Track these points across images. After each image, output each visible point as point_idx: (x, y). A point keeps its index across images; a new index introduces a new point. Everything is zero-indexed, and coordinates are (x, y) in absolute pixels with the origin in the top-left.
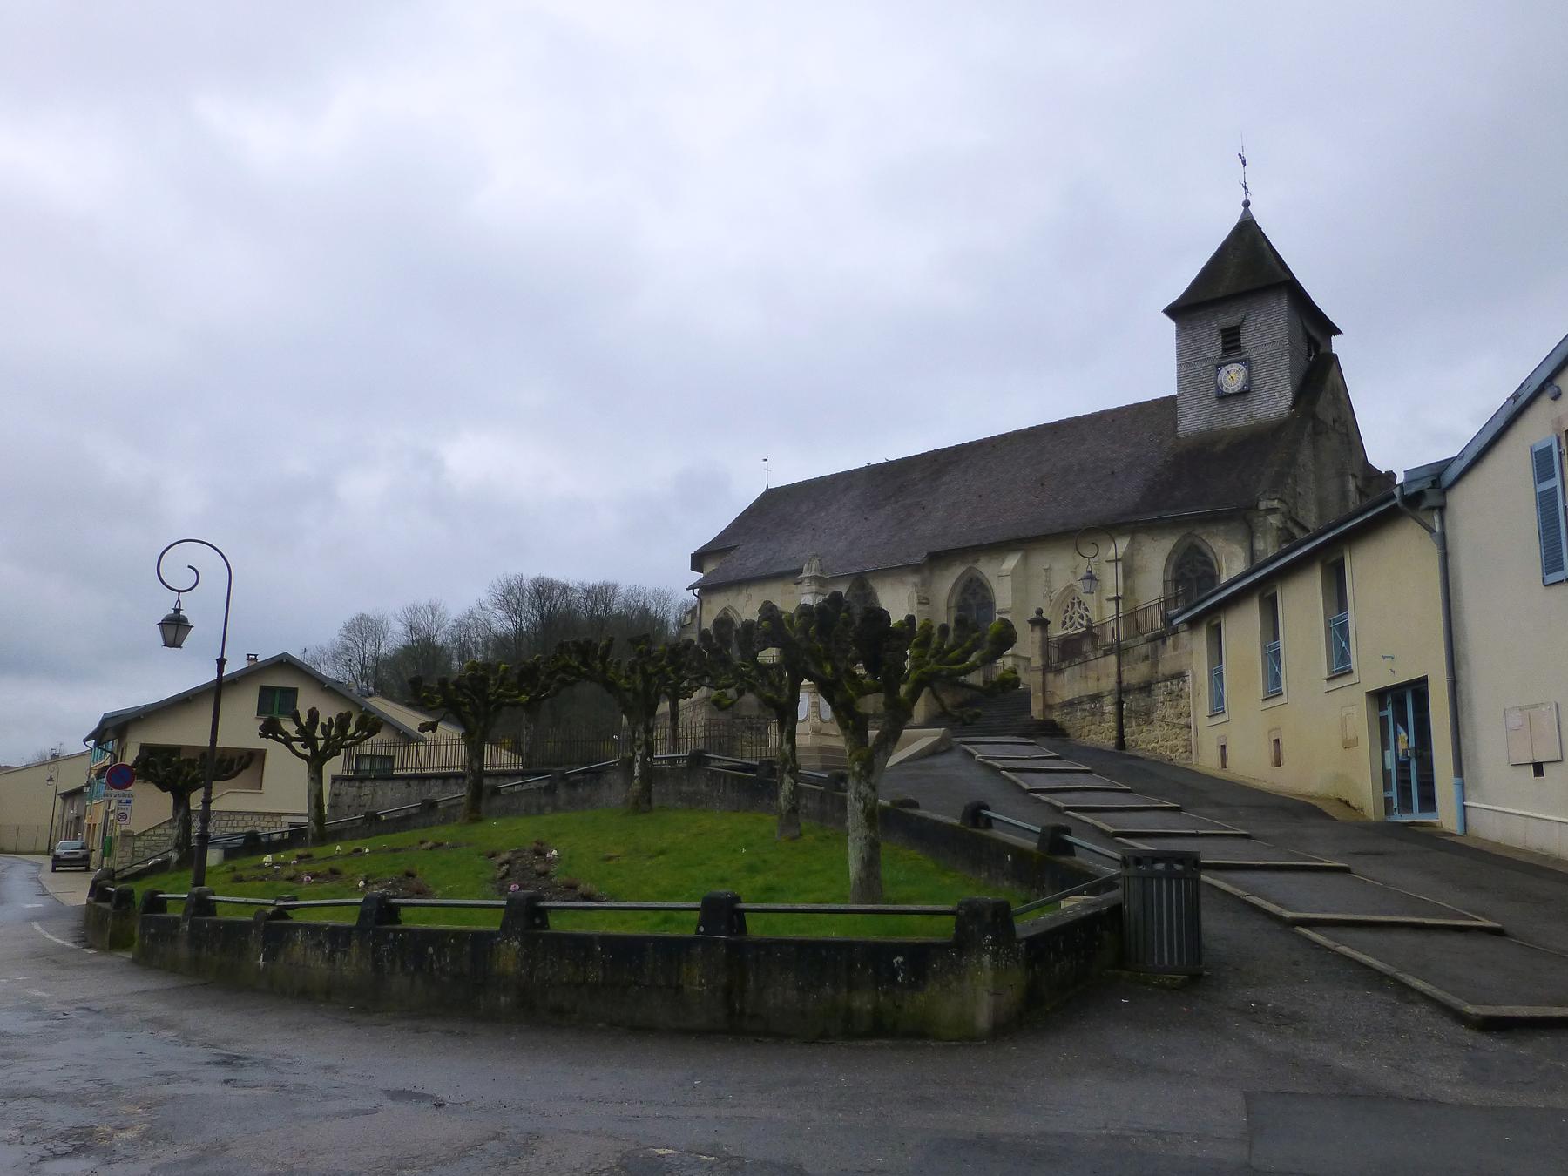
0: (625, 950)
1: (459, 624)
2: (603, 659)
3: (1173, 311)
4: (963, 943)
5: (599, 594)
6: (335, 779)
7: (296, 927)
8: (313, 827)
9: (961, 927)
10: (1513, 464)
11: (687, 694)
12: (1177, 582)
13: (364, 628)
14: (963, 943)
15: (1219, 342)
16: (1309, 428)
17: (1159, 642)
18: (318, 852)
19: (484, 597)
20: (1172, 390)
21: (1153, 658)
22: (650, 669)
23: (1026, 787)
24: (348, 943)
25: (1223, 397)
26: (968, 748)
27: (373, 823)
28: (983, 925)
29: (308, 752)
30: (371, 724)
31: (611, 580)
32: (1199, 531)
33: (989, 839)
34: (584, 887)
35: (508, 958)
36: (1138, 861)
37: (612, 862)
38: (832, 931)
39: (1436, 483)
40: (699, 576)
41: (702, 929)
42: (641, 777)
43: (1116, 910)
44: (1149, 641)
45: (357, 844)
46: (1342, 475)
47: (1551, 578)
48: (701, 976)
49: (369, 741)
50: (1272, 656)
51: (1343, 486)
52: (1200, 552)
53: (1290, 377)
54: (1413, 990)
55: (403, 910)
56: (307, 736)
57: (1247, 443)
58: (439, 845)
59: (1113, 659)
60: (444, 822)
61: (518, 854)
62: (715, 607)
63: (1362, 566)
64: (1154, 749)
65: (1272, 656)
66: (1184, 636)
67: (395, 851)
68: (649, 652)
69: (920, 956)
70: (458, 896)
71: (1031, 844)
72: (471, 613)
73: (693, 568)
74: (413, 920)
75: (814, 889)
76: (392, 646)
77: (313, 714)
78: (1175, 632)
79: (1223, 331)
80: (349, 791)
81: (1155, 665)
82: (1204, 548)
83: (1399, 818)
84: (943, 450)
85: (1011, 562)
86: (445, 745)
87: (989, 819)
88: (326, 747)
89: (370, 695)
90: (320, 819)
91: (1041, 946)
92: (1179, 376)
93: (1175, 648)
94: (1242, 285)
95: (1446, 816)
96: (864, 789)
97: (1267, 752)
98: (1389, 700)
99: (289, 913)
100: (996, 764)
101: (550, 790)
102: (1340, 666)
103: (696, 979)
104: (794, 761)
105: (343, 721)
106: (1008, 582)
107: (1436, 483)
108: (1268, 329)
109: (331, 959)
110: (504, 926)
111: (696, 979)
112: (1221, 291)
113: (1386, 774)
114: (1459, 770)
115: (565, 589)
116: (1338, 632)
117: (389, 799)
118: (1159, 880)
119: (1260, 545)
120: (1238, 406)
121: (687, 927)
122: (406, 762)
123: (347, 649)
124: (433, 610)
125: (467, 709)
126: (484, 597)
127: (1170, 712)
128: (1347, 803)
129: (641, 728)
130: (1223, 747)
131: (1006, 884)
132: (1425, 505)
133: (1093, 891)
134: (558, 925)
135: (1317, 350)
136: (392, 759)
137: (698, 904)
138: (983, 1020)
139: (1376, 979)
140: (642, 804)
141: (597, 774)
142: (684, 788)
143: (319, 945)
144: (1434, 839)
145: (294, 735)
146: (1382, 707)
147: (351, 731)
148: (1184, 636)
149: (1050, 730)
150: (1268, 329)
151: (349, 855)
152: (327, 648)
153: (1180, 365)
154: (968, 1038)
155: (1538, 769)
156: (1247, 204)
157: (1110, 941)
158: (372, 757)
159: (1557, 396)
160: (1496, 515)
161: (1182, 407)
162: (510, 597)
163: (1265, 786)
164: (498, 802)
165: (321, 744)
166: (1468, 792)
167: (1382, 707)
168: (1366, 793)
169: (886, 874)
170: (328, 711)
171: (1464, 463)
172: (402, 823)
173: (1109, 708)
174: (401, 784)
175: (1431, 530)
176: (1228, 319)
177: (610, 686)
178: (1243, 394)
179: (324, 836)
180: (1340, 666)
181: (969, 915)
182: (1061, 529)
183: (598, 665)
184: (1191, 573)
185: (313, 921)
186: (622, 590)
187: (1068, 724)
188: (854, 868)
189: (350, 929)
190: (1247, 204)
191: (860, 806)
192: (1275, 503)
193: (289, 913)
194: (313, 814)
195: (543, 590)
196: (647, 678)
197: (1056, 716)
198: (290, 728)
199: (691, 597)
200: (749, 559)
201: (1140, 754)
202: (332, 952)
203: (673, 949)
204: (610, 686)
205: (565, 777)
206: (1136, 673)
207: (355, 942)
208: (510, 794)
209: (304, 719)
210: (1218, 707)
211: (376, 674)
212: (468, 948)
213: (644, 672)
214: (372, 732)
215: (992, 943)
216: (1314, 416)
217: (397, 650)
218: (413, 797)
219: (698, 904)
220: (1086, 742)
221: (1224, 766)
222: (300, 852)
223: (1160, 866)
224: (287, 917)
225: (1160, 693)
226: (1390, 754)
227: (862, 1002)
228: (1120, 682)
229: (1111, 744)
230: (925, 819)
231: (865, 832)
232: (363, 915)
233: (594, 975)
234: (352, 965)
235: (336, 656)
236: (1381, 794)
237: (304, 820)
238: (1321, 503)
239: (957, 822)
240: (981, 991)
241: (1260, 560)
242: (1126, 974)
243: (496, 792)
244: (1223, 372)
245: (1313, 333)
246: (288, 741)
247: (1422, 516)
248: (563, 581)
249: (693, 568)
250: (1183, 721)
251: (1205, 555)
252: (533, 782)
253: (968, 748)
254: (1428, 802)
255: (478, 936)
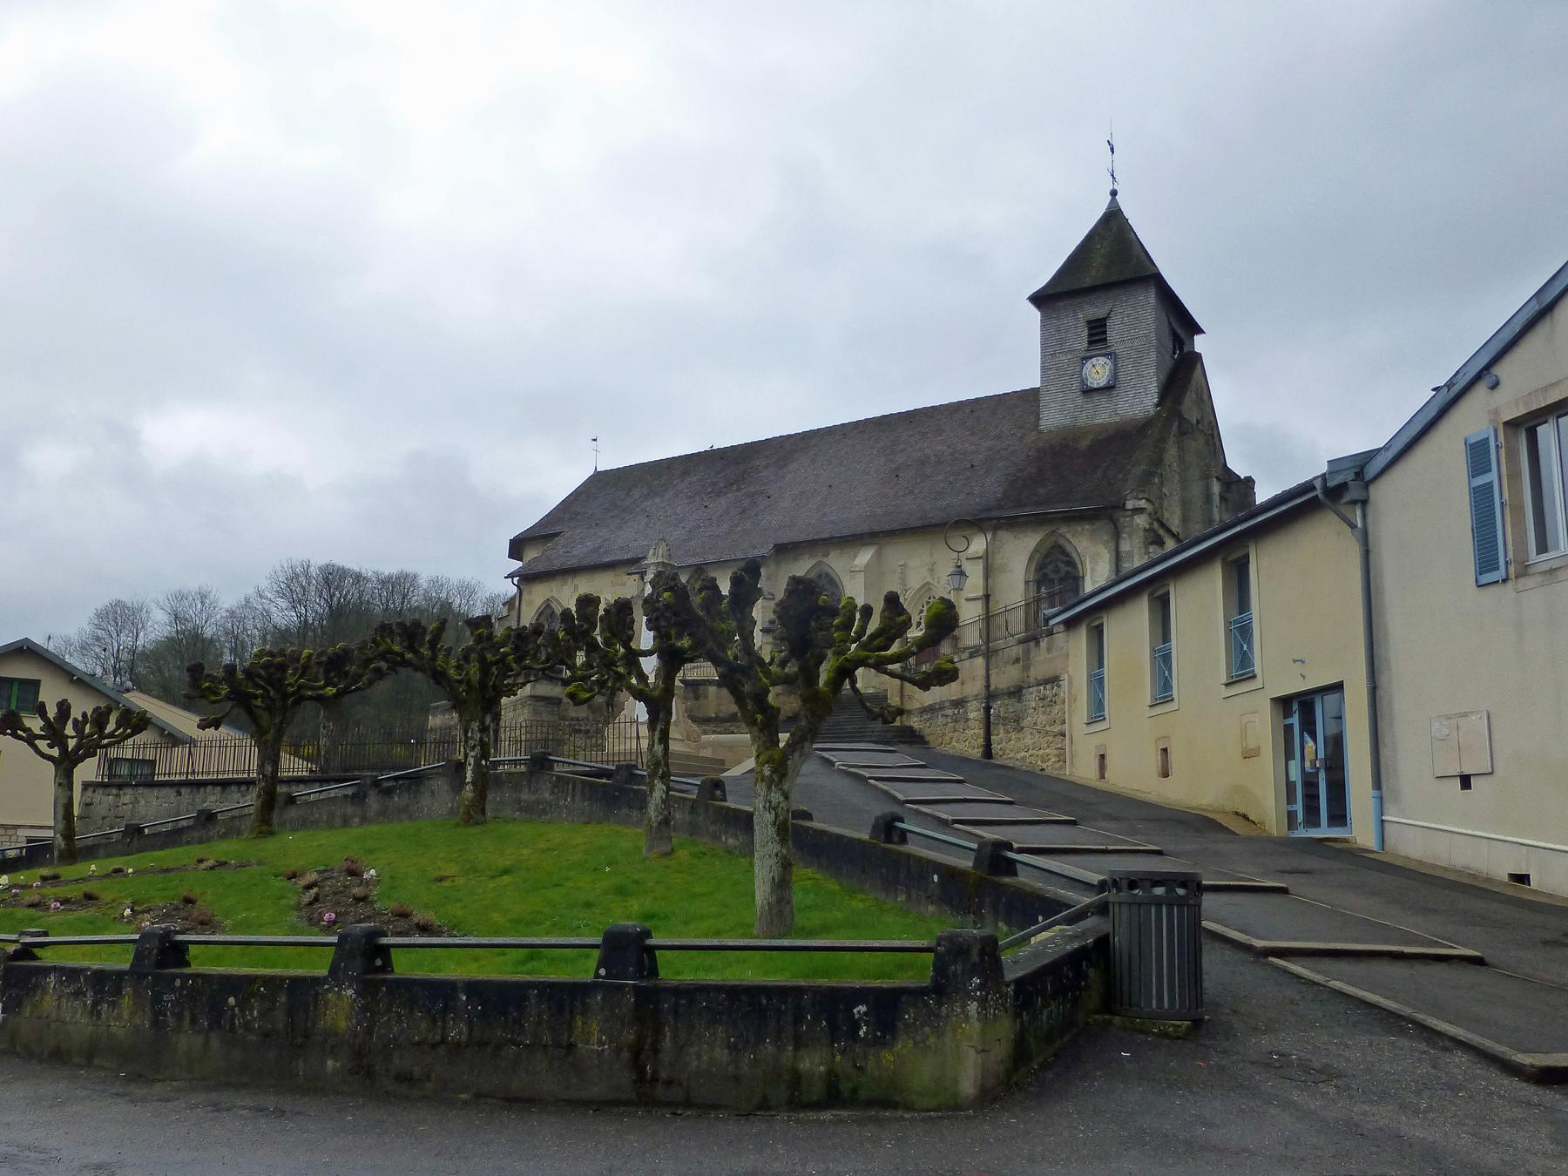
0: (499, 1000)
1: (232, 613)
2: (433, 644)
3: (1038, 299)
4: (942, 988)
5: (399, 584)
6: (86, 786)
7: (46, 971)
8: (60, 842)
9: (940, 968)
10: (1446, 452)
11: (511, 692)
12: (1039, 583)
13: (120, 616)
14: (942, 988)
15: (1086, 333)
16: (1175, 428)
17: (1032, 644)
18: (67, 872)
19: (264, 584)
20: (1034, 381)
21: (1024, 661)
22: (489, 656)
23: (901, 797)
24: (118, 992)
25: (1088, 392)
26: (826, 755)
27: (134, 837)
28: (962, 967)
29: (55, 752)
30: (136, 722)
31: (410, 568)
32: (1063, 530)
33: (909, 856)
34: (419, 916)
35: (340, 1009)
36: (1132, 885)
37: (446, 884)
38: (749, 972)
39: (1359, 475)
40: (516, 565)
41: (602, 972)
42: (473, 783)
43: (1103, 943)
44: (1020, 642)
45: (117, 862)
46: (1206, 477)
47: (1485, 579)
48: (601, 1031)
49: (130, 741)
50: (1163, 660)
51: (1208, 488)
52: (1064, 552)
53: (1157, 374)
54: (1439, 1034)
55: (193, 949)
56: (54, 733)
57: (1107, 440)
58: (222, 864)
59: (980, 661)
60: (224, 836)
61: (326, 873)
62: (539, 595)
63: (1270, 566)
64: (1024, 758)
65: (1163, 660)
66: (1060, 638)
67: (167, 871)
68: (490, 637)
69: (888, 1006)
70: (260, 931)
71: (966, 863)
72: (247, 601)
73: (510, 556)
74: (202, 963)
75: (721, 921)
76: (152, 636)
77: (64, 709)
78: (1050, 633)
79: (1089, 322)
80: (104, 800)
81: (1027, 668)
82: (1069, 548)
83: (1302, 833)
84: (789, 436)
85: (864, 557)
86: (228, 751)
87: (904, 832)
88: (78, 747)
89: (128, 690)
90: (69, 834)
91: (1028, 991)
92: (1043, 368)
93: (1049, 650)
94: (1106, 276)
95: (1361, 830)
96: (776, 797)
97: (1154, 761)
98: (1295, 707)
99: (36, 951)
100: (865, 773)
101: (359, 798)
102: (1241, 669)
103: (594, 1035)
104: (667, 765)
105: (100, 719)
106: (861, 578)
107: (1359, 475)
108: (1134, 321)
109: (94, 1012)
110: (334, 971)
111: (594, 1035)
112: (1088, 281)
113: (1290, 787)
114: (1377, 783)
115: (358, 578)
116: (1240, 632)
117: (153, 809)
118: (1159, 905)
119: (1125, 546)
120: (1102, 400)
121: (585, 969)
122: (173, 765)
123: (98, 639)
124: (203, 597)
125: (259, 702)
126: (264, 584)
127: (1042, 718)
128: (1245, 817)
129: (475, 725)
130: (1103, 757)
131: (931, 908)
132: (1347, 497)
133: (1071, 920)
134: (405, 966)
135: (1181, 349)
136: (152, 763)
137: (598, 940)
138: (968, 1087)
139: (1394, 1022)
140: (475, 814)
141: (416, 780)
142: (525, 796)
143: (78, 994)
144: (1355, 856)
145: (37, 731)
146: (1287, 713)
147: (110, 727)
148: (1060, 638)
149: (912, 738)
150: (1134, 321)
151: (106, 876)
152: (75, 638)
153: (1044, 356)
154: (950, 1108)
155: (1466, 782)
156: (1114, 193)
157: (1105, 978)
158: (132, 761)
159: (1495, 386)
160: (1427, 514)
161: (1045, 399)
162: (294, 585)
163: (1153, 798)
164: (293, 813)
165: (72, 743)
166: (1386, 805)
167: (1287, 713)
168: (1268, 805)
169: (797, 897)
170: (82, 706)
171: (1390, 455)
172: (174, 837)
173: (974, 713)
174: (170, 793)
175: (1353, 526)
176: (1094, 311)
177: (439, 677)
178: (1109, 388)
179: (72, 854)
180: (1241, 669)
181: (950, 954)
182: (919, 523)
183: (425, 651)
184: (1056, 574)
185: (70, 964)
186: (423, 582)
187: (927, 731)
188: (762, 891)
189: (120, 974)
190: (1114, 193)
191: (770, 817)
192: (1143, 504)
193: (36, 951)
194: (61, 826)
195: (333, 577)
196: (485, 667)
197: (915, 722)
198: (35, 724)
199: (510, 589)
200: (577, 545)
201: (1007, 763)
202: (95, 1004)
203: (565, 998)
204: (439, 677)
205: (376, 783)
206: (1005, 677)
207: (128, 990)
208: (307, 803)
209: (52, 712)
210: (1097, 712)
211: (132, 669)
212: (283, 999)
213: (482, 660)
214: (137, 730)
215: (981, 987)
216: (1180, 416)
217: (157, 642)
218: (187, 806)
219: (598, 940)
220: (947, 749)
221: (1102, 777)
222: (45, 872)
223: (1159, 891)
224: (35, 958)
225: (1031, 697)
226: (1294, 767)
227: (813, 1063)
228: (988, 686)
229: (976, 753)
230: (824, 833)
231: (776, 848)
232: (139, 957)
233: (457, 1031)
234: (125, 1018)
235: (84, 647)
236: (1284, 807)
237: (50, 834)
238: (1185, 505)
239: (865, 837)
240: (967, 1045)
241: (1127, 567)
242: (1117, 1020)
243: (291, 800)
244: (1089, 365)
245: (1179, 331)
246: (31, 739)
247: (1343, 509)
248: (357, 569)
249: (510, 556)
250: (1057, 729)
251: (1068, 555)
252: (334, 790)
253: (826, 755)
254: (1339, 816)
255: (296, 982)
